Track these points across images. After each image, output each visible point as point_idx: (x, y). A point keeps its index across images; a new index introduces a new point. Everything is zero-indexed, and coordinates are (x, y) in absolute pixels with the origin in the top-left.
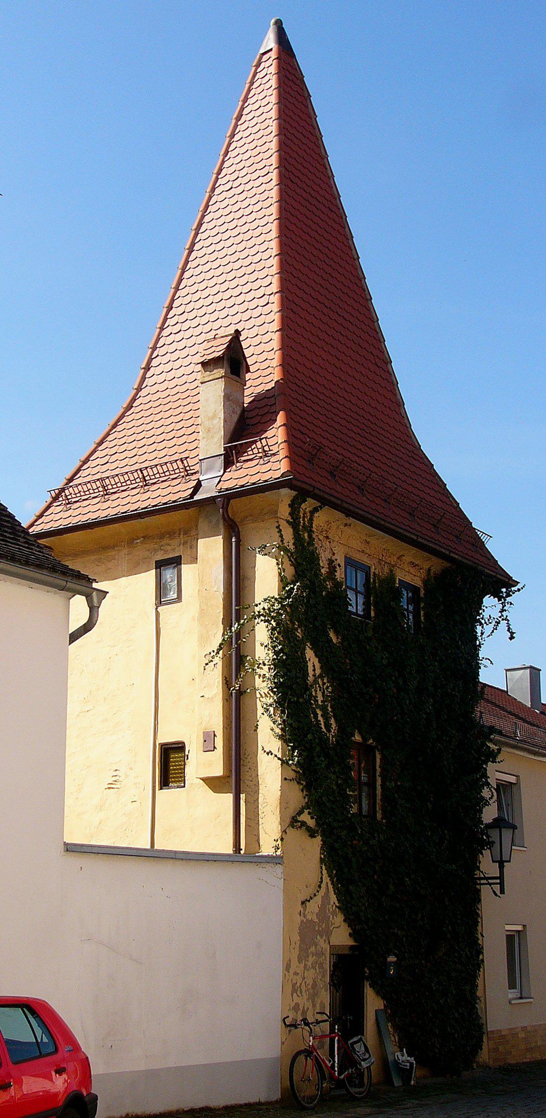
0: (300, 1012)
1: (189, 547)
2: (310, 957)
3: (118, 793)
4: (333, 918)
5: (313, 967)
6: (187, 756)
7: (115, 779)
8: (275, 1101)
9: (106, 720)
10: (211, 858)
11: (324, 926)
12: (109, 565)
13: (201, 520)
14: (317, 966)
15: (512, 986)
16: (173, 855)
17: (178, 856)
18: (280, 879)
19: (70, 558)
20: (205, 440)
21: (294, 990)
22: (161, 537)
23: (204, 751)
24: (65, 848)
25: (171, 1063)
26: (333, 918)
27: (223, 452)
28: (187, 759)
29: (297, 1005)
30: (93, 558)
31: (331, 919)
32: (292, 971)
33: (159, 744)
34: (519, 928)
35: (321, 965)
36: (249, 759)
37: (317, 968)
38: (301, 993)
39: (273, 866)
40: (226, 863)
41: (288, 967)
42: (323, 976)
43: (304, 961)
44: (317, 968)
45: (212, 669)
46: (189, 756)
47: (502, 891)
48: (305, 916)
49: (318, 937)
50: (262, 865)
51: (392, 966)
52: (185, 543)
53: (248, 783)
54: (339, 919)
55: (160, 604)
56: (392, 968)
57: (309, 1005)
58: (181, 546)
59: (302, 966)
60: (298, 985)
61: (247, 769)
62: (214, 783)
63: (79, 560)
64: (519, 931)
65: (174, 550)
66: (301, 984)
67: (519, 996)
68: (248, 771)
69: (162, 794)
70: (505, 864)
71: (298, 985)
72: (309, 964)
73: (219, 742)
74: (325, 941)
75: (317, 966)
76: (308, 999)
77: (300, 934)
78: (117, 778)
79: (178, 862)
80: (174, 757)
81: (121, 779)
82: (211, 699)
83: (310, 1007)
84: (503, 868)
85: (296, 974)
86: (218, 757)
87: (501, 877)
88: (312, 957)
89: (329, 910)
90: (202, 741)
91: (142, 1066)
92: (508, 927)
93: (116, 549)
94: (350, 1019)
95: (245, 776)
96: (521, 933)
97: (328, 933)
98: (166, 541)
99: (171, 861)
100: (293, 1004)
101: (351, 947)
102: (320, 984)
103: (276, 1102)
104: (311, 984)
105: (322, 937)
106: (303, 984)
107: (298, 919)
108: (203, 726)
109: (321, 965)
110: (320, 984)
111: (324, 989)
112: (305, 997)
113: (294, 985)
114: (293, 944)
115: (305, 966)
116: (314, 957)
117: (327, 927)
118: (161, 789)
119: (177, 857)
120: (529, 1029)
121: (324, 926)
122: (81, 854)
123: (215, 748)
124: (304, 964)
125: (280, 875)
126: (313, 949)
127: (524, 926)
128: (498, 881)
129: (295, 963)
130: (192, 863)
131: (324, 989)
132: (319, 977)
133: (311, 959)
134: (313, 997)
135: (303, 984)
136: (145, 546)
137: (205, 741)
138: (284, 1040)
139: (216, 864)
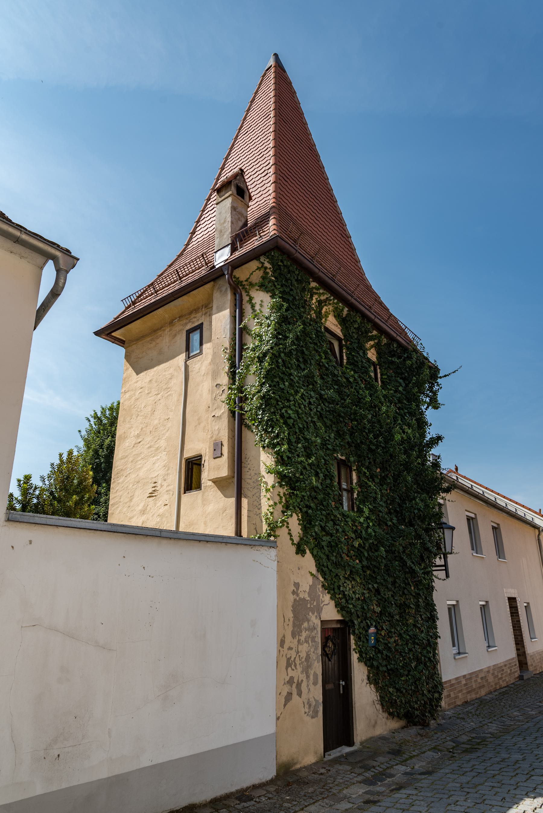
0: (294, 686)
1: (208, 316)
2: (303, 632)
3: (155, 500)
4: (323, 597)
5: (307, 642)
6: (203, 464)
7: (154, 489)
8: (270, 781)
9: (150, 447)
10: (203, 538)
11: (315, 604)
12: (158, 341)
13: (215, 291)
14: (310, 640)
15: (454, 645)
16: (158, 534)
17: (163, 534)
18: (274, 561)
19: (135, 342)
20: (218, 239)
21: (289, 665)
22: (191, 313)
23: (214, 458)
24: (6, 517)
25: (145, 762)
26: (323, 597)
27: (230, 242)
28: (203, 467)
29: (292, 678)
30: (148, 339)
31: (321, 597)
32: (286, 646)
33: (185, 458)
34: (454, 603)
35: (313, 640)
36: (249, 462)
37: (310, 642)
38: (295, 666)
39: (267, 550)
40: (219, 544)
41: (282, 643)
42: (316, 649)
43: (297, 637)
44: (310, 642)
45: (220, 394)
46: (205, 465)
47: (447, 576)
48: (298, 595)
49: (310, 614)
50: (257, 548)
51: (373, 636)
52: (206, 313)
53: (248, 481)
54: (327, 598)
55: (189, 358)
56: (373, 638)
57: (303, 677)
58: (203, 316)
59: (296, 641)
60: (292, 659)
61: (247, 470)
62: (219, 483)
63: (140, 343)
64: (454, 605)
65: (198, 320)
66: (295, 658)
67: (458, 652)
68: (248, 472)
69: (187, 498)
70: (448, 556)
71: (292, 659)
72: (302, 638)
73: (225, 450)
74: (316, 617)
75: (310, 640)
76: (302, 672)
77: (294, 611)
78: (156, 488)
79: (165, 541)
80: (195, 467)
81: (158, 489)
82: (220, 417)
83: (305, 679)
84: (447, 558)
85: (290, 648)
86: (224, 460)
87: (446, 565)
88: (305, 632)
89: (319, 589)
90: (213, 450)
91: (104, 774)
92: (449, 603)
93: (163, 329)
94: (342, 684)
95: (246, 475)
96: (455, 606)
97: (319, 610)
98: (193, 315)
99: (156, 540)
100: (287, 679)
101: (338, 621)
102: (313, 656)
103: (272, 782)
104: (305, 657)
105: (313, 613)
106: (297, 659)
107: (292, 598)
108: (214, 439)
109: (313, 640)
110: (313, 656)
111: (316, 661)
112: (300, 669)
113: (288, 659)
114: (287, 620)
115: (299, 641)
116: (307, 632)
117: (318, 604)
118: (185, 493)
119: (162, 536)
120: (467, 677)
121: (315, 604)
122: (28, 526)
123: (222, 454)
124: (297, 639)
125: (274, 558)
126: (305, 625)
127: (457, 601)
128: (444, 568)
129: (289, 640)
130: (182, 543)
131: (316, 661)
132: (312, 650)
133: (304, 634)
134: (306, 670)
135: (297, 659)
136: (180, 323)
137: (215, 450)
138: (279, 715)
139: (209, 545)
